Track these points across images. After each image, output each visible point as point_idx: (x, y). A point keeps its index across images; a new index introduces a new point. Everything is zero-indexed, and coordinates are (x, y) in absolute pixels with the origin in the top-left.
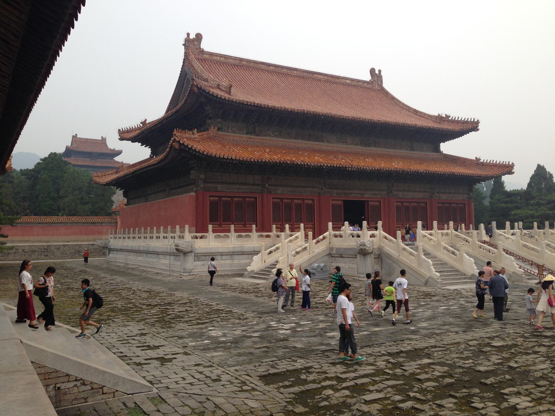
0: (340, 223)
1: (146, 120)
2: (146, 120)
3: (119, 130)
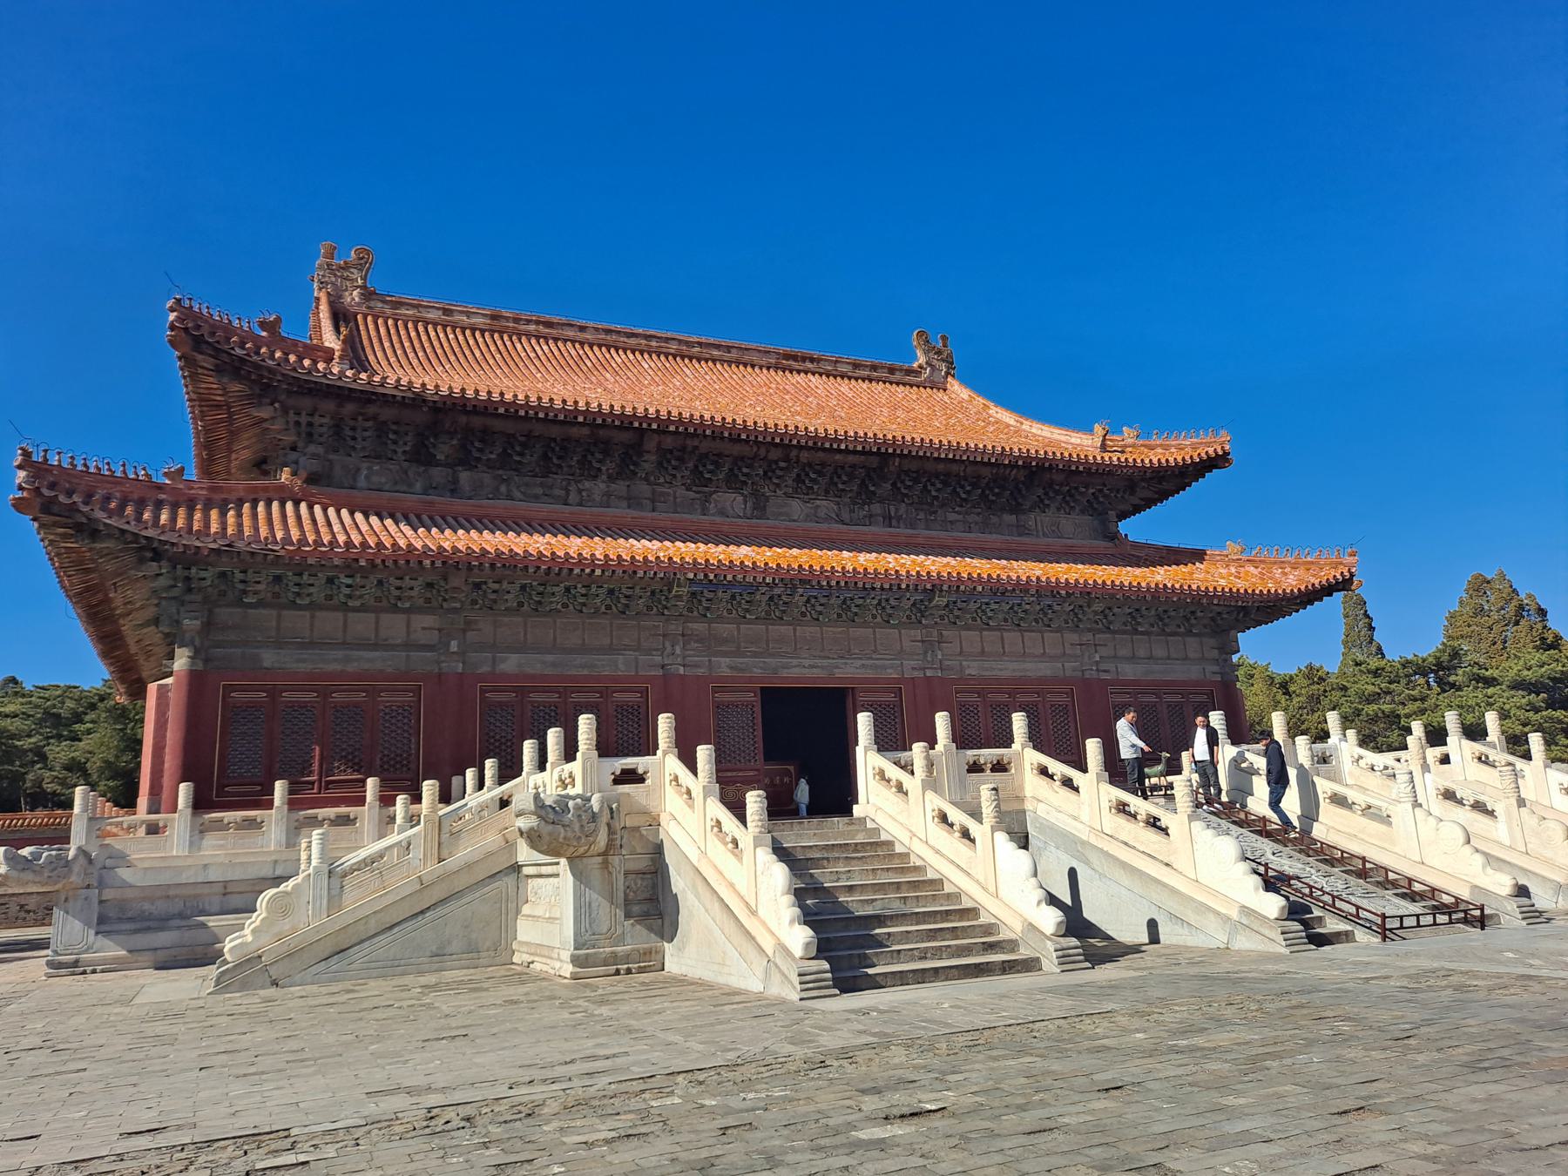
3: (26, 454)
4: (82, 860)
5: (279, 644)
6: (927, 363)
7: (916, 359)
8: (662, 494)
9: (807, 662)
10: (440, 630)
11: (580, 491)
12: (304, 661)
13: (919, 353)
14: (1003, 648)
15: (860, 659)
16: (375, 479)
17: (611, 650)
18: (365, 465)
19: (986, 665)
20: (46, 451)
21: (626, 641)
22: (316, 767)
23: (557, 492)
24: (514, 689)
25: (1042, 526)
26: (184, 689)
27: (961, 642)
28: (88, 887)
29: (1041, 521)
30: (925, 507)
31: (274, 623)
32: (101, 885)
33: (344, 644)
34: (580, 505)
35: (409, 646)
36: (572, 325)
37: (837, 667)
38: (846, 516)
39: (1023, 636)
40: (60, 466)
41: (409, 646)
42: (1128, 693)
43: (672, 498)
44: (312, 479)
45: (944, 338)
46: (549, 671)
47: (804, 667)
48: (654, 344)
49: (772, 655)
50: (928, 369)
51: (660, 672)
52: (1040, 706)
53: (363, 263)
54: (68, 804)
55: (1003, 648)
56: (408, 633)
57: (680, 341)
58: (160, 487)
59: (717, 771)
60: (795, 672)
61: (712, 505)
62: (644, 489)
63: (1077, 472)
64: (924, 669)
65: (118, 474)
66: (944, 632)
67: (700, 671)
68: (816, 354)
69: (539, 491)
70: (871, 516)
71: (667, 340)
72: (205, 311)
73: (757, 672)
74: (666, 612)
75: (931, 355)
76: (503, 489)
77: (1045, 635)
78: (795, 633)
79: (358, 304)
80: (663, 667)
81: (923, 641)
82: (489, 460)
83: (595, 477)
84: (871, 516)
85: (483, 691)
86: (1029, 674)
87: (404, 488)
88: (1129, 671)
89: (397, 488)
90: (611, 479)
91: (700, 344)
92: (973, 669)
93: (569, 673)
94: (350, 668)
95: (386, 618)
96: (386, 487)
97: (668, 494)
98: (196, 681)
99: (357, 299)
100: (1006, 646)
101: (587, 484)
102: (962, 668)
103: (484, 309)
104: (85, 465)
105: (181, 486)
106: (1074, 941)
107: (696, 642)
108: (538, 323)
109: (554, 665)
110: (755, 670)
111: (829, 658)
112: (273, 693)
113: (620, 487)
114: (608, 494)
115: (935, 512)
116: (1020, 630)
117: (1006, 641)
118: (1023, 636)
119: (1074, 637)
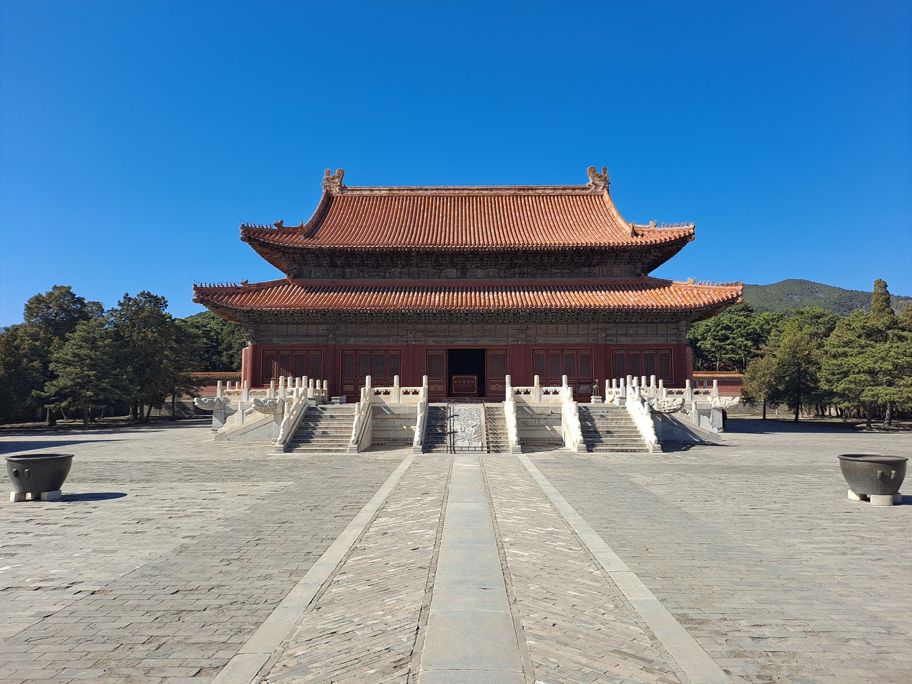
0: (351, 378)
1: (282, 222)
2: (282, 222)
3: (195, 286)
4: (218, 402)
5: (278, 336)
6: (593, 183)
7: (589, 181)
8: (422, 271)
9: (465, 339)
10: (328, 330)
11: (390, 273)
12: (285, 341)
13: (590, 178)
14: (557, 331)
15: (489, 337)
16: (317, 274)
17: (388, 336)
18: (314, 269)
19: (549, 339)
20: (201, 284)
21: (393, 333)
22: (275, 375)
23: (381, 274)
24: (354, 350)
25: (602, 272)
26: (251, 351)
27: (536, 329)
28: (221, 409)
29: (602, 269)
30: (542, 267)
31: (276, 329)
32: (224, 409)
33: (298, 336)
34: (390, 278)
35: (318, 336)
36: (422, 189)
37: (478, 341)
38: (502, 275)
39: (567, 326)
40: (206, 287)
41: (318, 336)
42: (624, 350)
43: (426, 273)
44: (295, 277)
45: (605, 169)
46: (365, 344)
47: (464, 341)
48: (457, 192)
49: (452, 337)
50: (593, 186)
51: (406, 344)
52: (575, 355)
53: (341, 175)
54: (270, 383)
55: (557, 331)
56: (317, 331)
57: (469, 190)
58: (239, 288)
59: (428, 380)
60: (460, 343)
61: (443, 274)
62: (414, 270)
63: (605, 250)
64: (518, 341)
65: (225, 286)
66: (528, 326)
67: (421, 343)
68: (534, 186)
69: (375, 274)
70: (515, 273)
71: (463, 190)
72: (253, 226)
73: (444, 343)
74: (409, 321)
75: (596, 178)
76: (361, 274)
77: (579, 325)
78: (461, 328)
79: (338, 193)
80: (407, 341)
81: (518, 330)
82: (356, 263)
83: (396, 266)
84: (515, 273)
85: (613, 350)
86: (569, 342)
87: (327, 277)
88: (623, 340)
89: (325, 277)
90: (403, 266)
91: (478, 190)
92: (541, 341)
93: (373, 344)
94: (299, 343)
95: (310, 326)
96: (320, 277)
97: (425, 271)
98: (255, 348)
99: (338, 191)
100: (559, 330)
101: (393, 270)
102: (536, 340)
103: (386, 187)
104: (214, 285)
105: (247, 287)
106: (520, 446)
107: (420, 332)
108: (408, 190)
109: (367, 341)
110: (443, 342)
111: (476, 337)
112: (278, 351)
113: (406, 270)
114: (400, 273)
115: (547, 269)
116: (567, 324)
117: (559, 329)
118: (567, 326)
119: (595, 326)
